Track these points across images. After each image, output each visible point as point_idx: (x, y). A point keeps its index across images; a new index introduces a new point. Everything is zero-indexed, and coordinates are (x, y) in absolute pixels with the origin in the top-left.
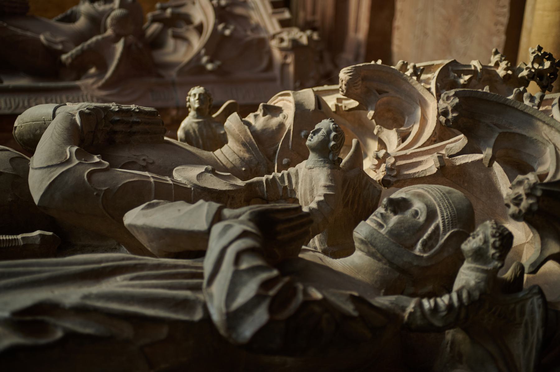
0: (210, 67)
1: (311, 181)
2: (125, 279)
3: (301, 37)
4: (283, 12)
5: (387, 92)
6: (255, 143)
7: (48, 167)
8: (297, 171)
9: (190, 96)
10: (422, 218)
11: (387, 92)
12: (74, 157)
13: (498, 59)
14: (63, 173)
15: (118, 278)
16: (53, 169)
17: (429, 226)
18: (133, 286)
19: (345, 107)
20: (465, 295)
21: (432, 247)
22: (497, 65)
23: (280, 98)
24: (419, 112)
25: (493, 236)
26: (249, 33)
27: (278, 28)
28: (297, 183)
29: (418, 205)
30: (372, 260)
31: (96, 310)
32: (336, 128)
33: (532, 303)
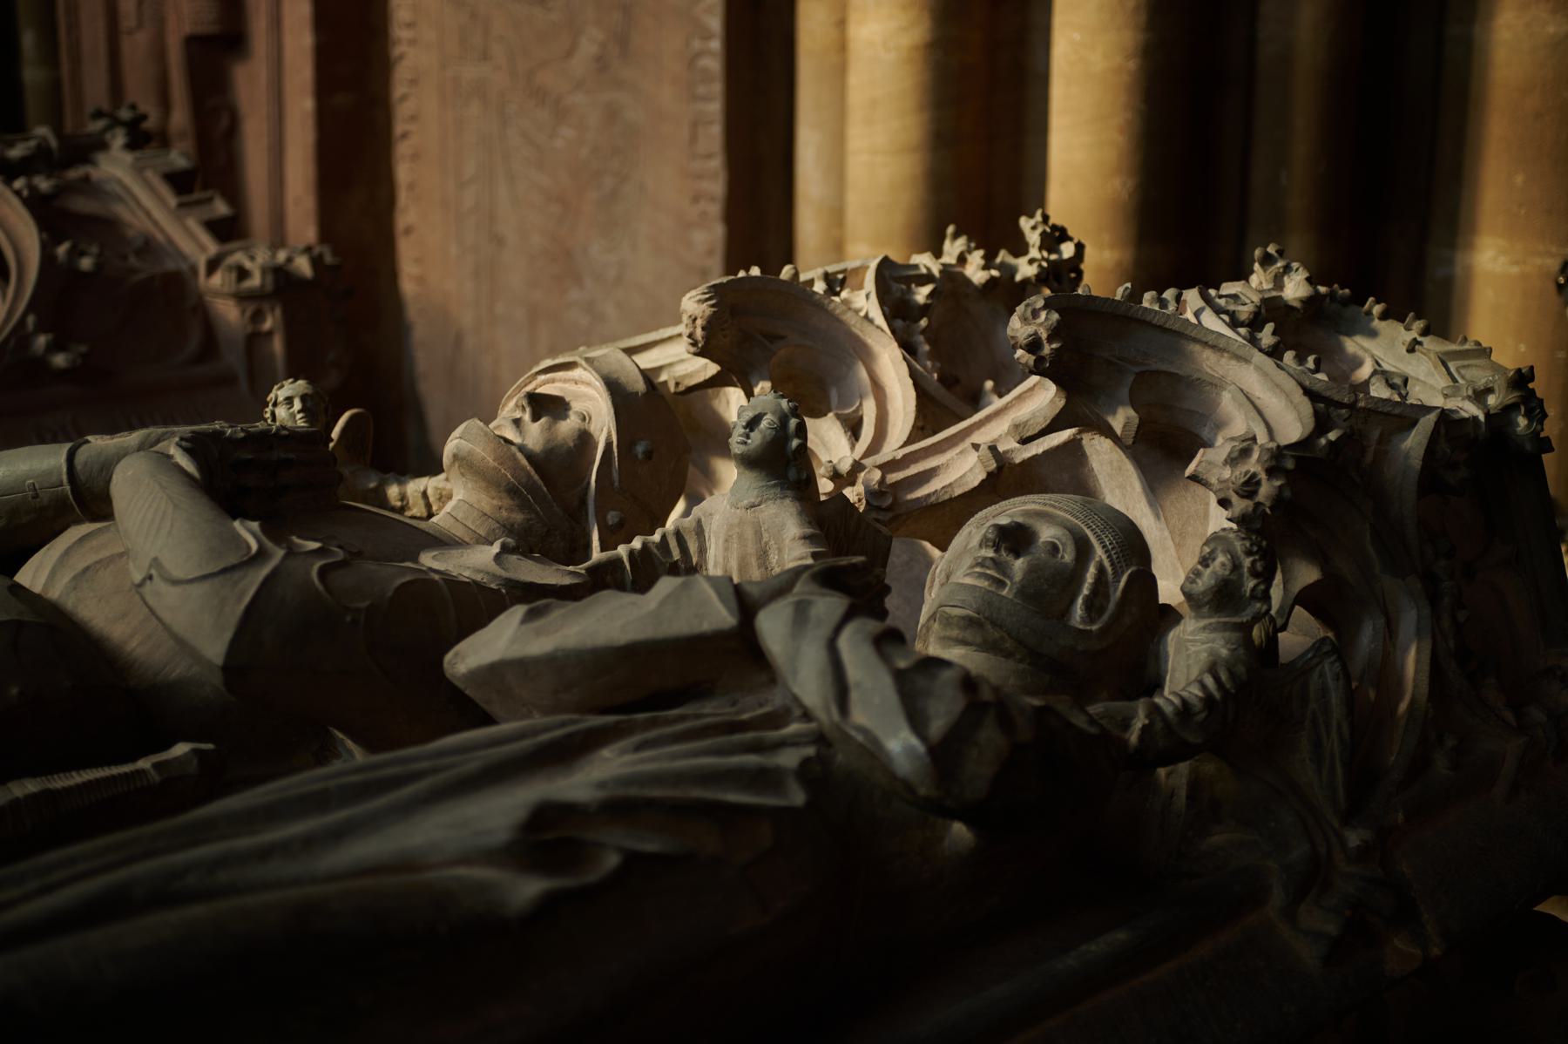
0: (60, 360)
1: (758, 534)
2: (623, 752)
3: (290, 260)
4: (210, 200)
5: (782, 338)
6: (540, 482)
7: (224, 571)
8: (699, 522)
9: (275, 404)
10: (1068, 556)
11: (782, 338)
12: (269, 544)
13: (963, 248)
14: (267, 580)
15: (606, 753)
16: (237, 575)
17: (1085, 569)
18: (642, 761)
19: (677, 384)
20: (1224, 677)
21: (1102, 610)
22: (962, 259)
23: (542, 377)
24: (863, 373)
25: (1249, 553)
26: (133, 261)
27: (213, 248)
28: (702, 550)
29: (1047, 533)
30: (991, 656)
31: (651, 803)
32: (796, 408)
33: (1322, 675)
